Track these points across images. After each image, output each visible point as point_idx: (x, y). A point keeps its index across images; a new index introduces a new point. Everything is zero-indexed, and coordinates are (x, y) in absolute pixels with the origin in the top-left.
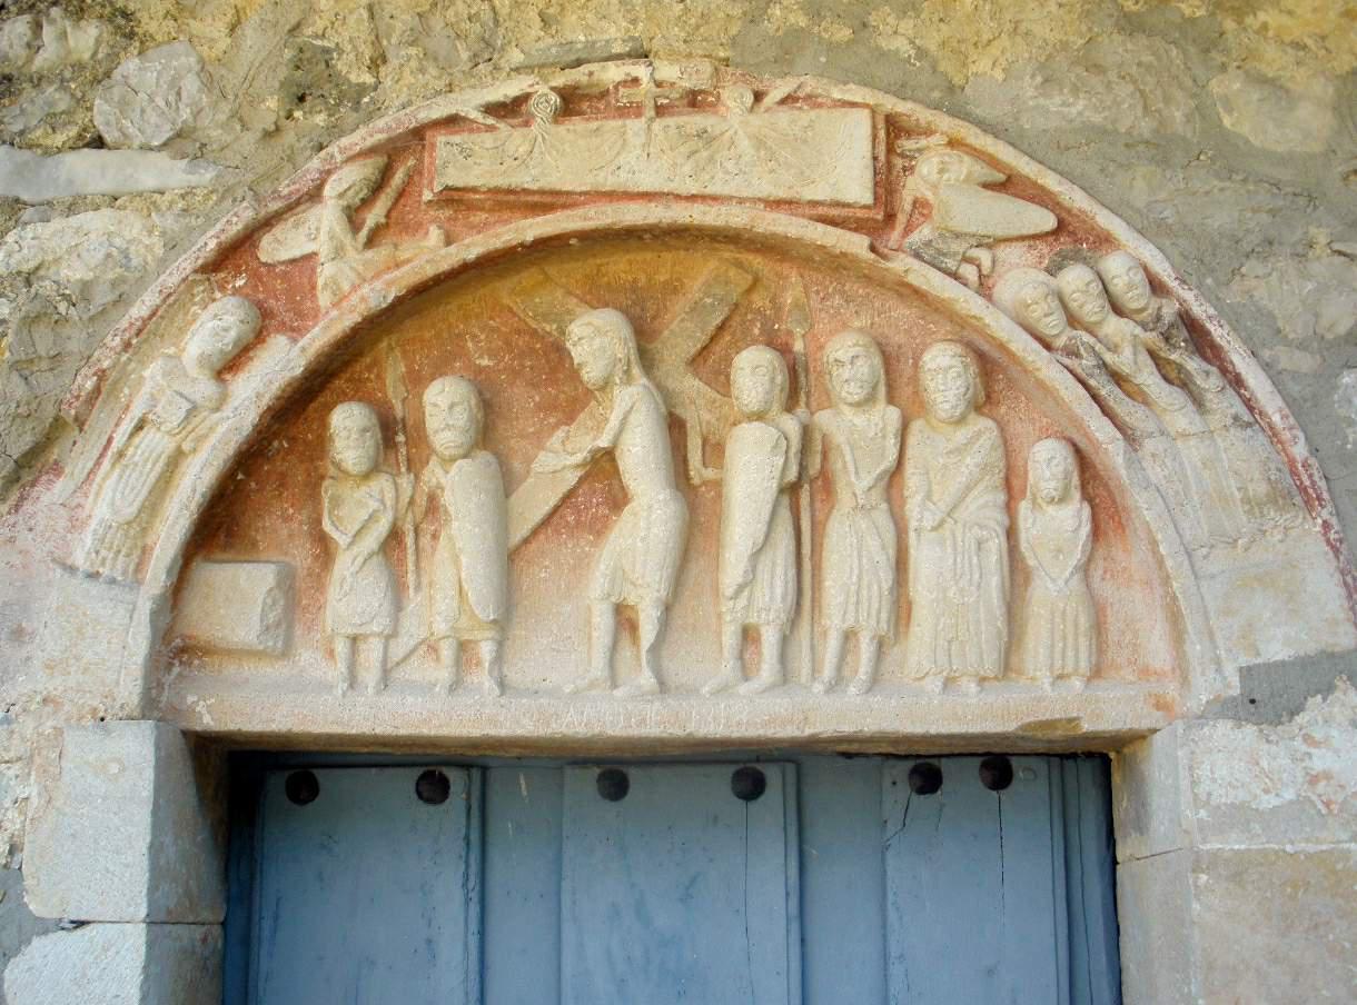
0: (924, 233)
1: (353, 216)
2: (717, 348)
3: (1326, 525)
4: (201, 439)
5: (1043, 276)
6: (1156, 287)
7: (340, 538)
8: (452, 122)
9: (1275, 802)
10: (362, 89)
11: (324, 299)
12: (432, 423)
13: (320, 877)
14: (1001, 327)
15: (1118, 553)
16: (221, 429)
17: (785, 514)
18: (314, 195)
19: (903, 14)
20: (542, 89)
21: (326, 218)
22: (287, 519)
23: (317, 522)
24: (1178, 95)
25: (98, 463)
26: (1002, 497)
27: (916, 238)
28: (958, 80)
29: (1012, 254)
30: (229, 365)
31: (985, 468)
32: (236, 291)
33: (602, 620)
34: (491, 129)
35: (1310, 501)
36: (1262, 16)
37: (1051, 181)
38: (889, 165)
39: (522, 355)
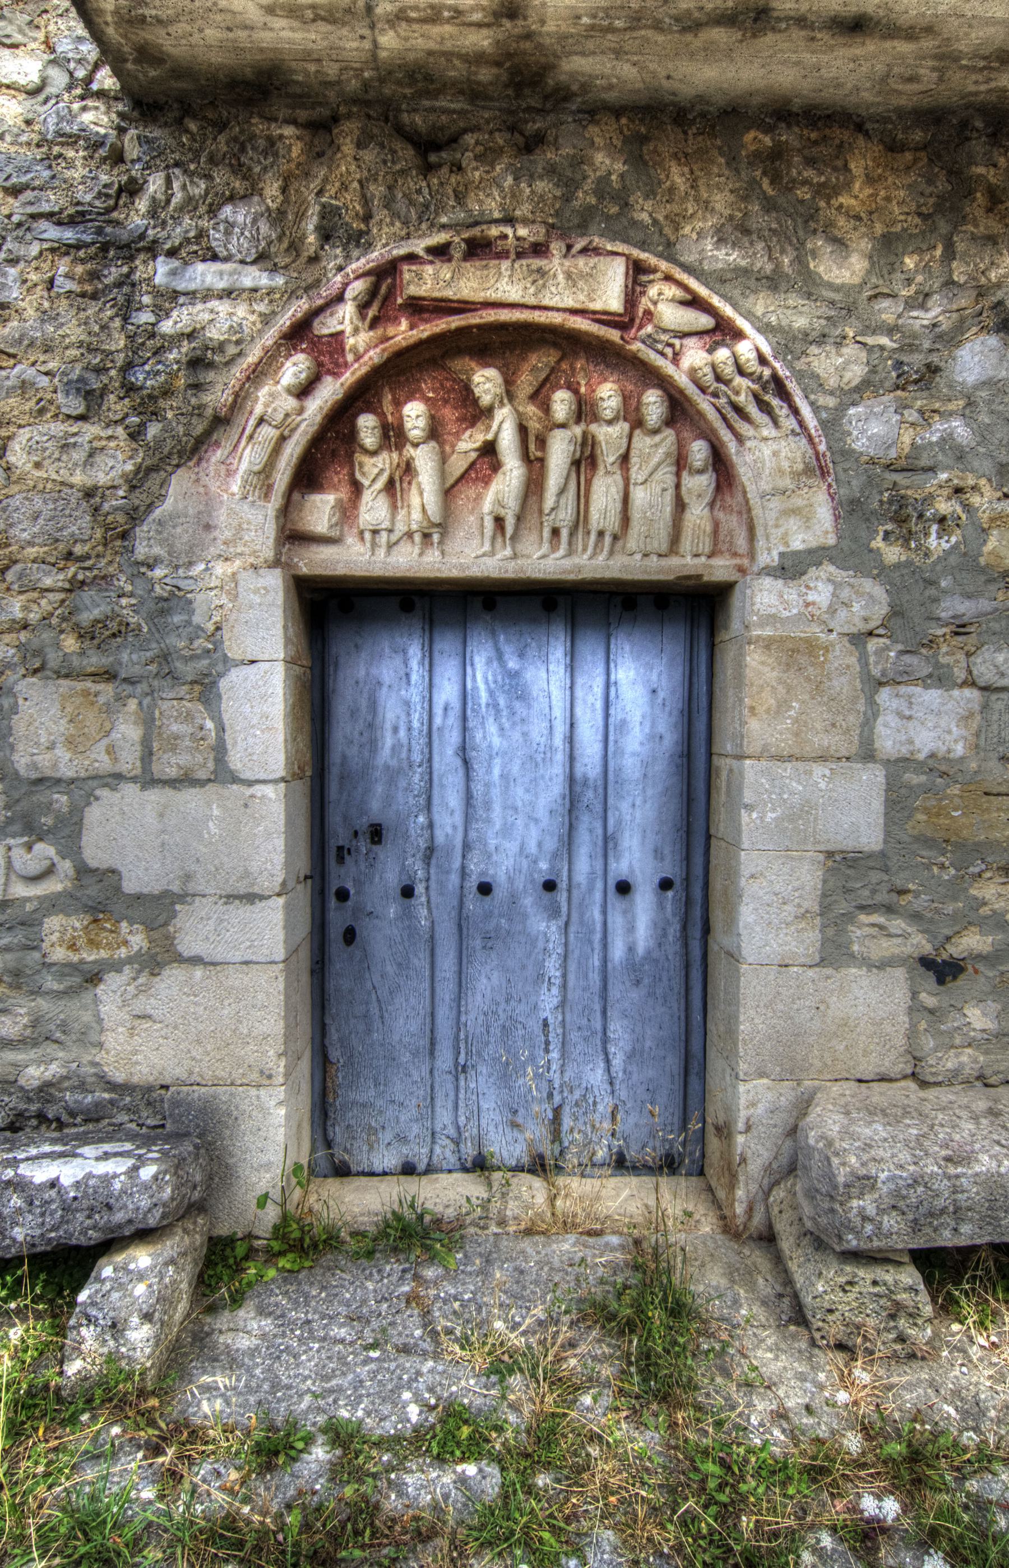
0: (649, 329)
1: (362, 308)
2: (544, 390)
3: (830, 486)
4: (293, 430)
5: (705, 355)
6: (762, 360)
7: (366, 482)
8: (411, 258)
9: (788, 614)
10: (361, 234)
11: (350, 357)
12: (408, 425)
13: (356, 646)
14: (682, 380)
15: (728, 499)
16: (303, 426)
17: (574, 475)
18: (339, 298)
19: (647, 197)
20: (457, 239)
21: (347, 310)
22: (337, 473)
23: (352, 475)
24: (789, 248)
25: (239, 441)
26: (674, 469)
27: (643, 332)
28: (673, 238)
29: (691, 342)
30: (304, 391)
31: (668, 455)
32: (303, 351)
33: (489, 524)
34: (431, 262)
35: (824, 473)
36: (841, 200)
37: (716, 301)
38: (633, 290)
39: (448, 392)
